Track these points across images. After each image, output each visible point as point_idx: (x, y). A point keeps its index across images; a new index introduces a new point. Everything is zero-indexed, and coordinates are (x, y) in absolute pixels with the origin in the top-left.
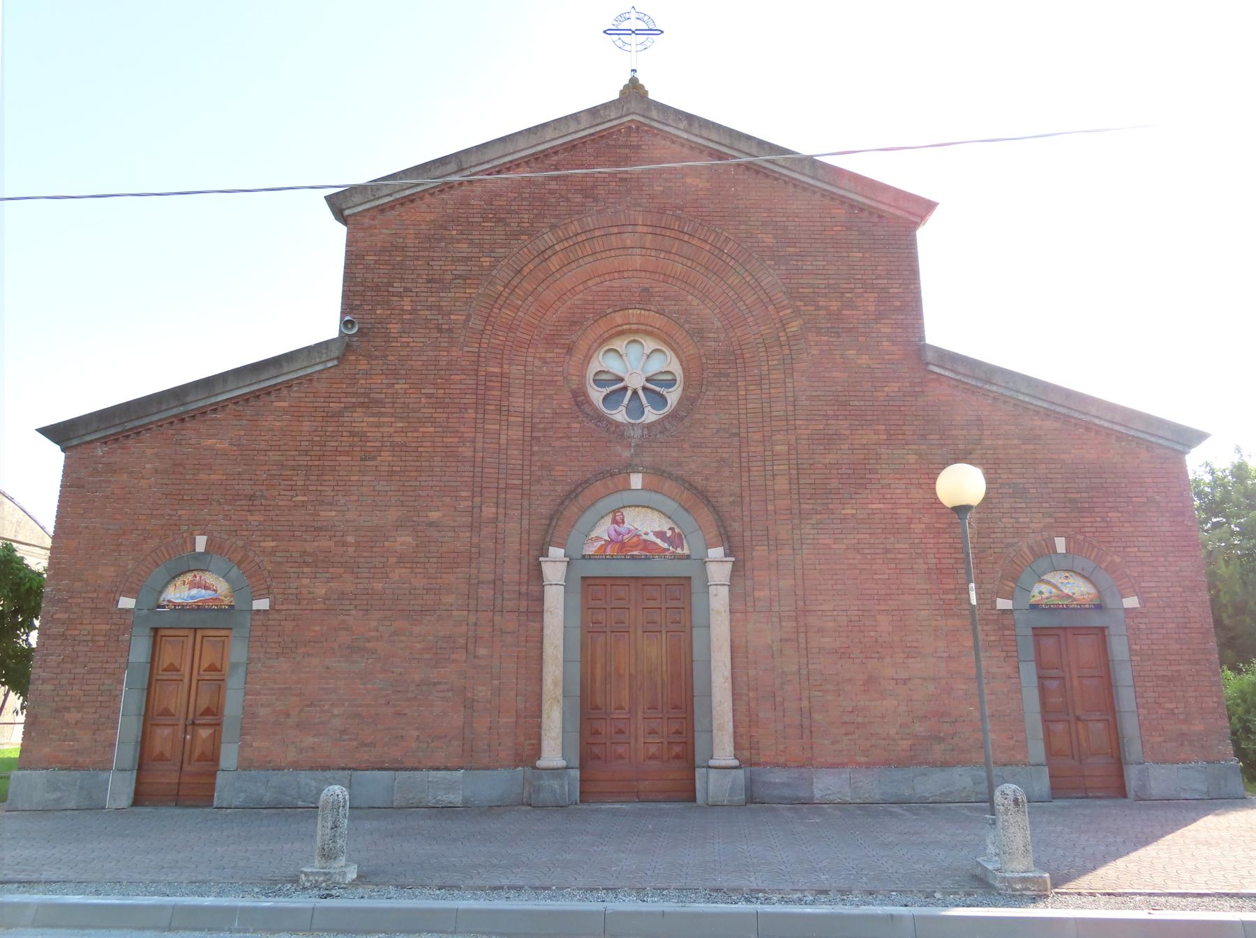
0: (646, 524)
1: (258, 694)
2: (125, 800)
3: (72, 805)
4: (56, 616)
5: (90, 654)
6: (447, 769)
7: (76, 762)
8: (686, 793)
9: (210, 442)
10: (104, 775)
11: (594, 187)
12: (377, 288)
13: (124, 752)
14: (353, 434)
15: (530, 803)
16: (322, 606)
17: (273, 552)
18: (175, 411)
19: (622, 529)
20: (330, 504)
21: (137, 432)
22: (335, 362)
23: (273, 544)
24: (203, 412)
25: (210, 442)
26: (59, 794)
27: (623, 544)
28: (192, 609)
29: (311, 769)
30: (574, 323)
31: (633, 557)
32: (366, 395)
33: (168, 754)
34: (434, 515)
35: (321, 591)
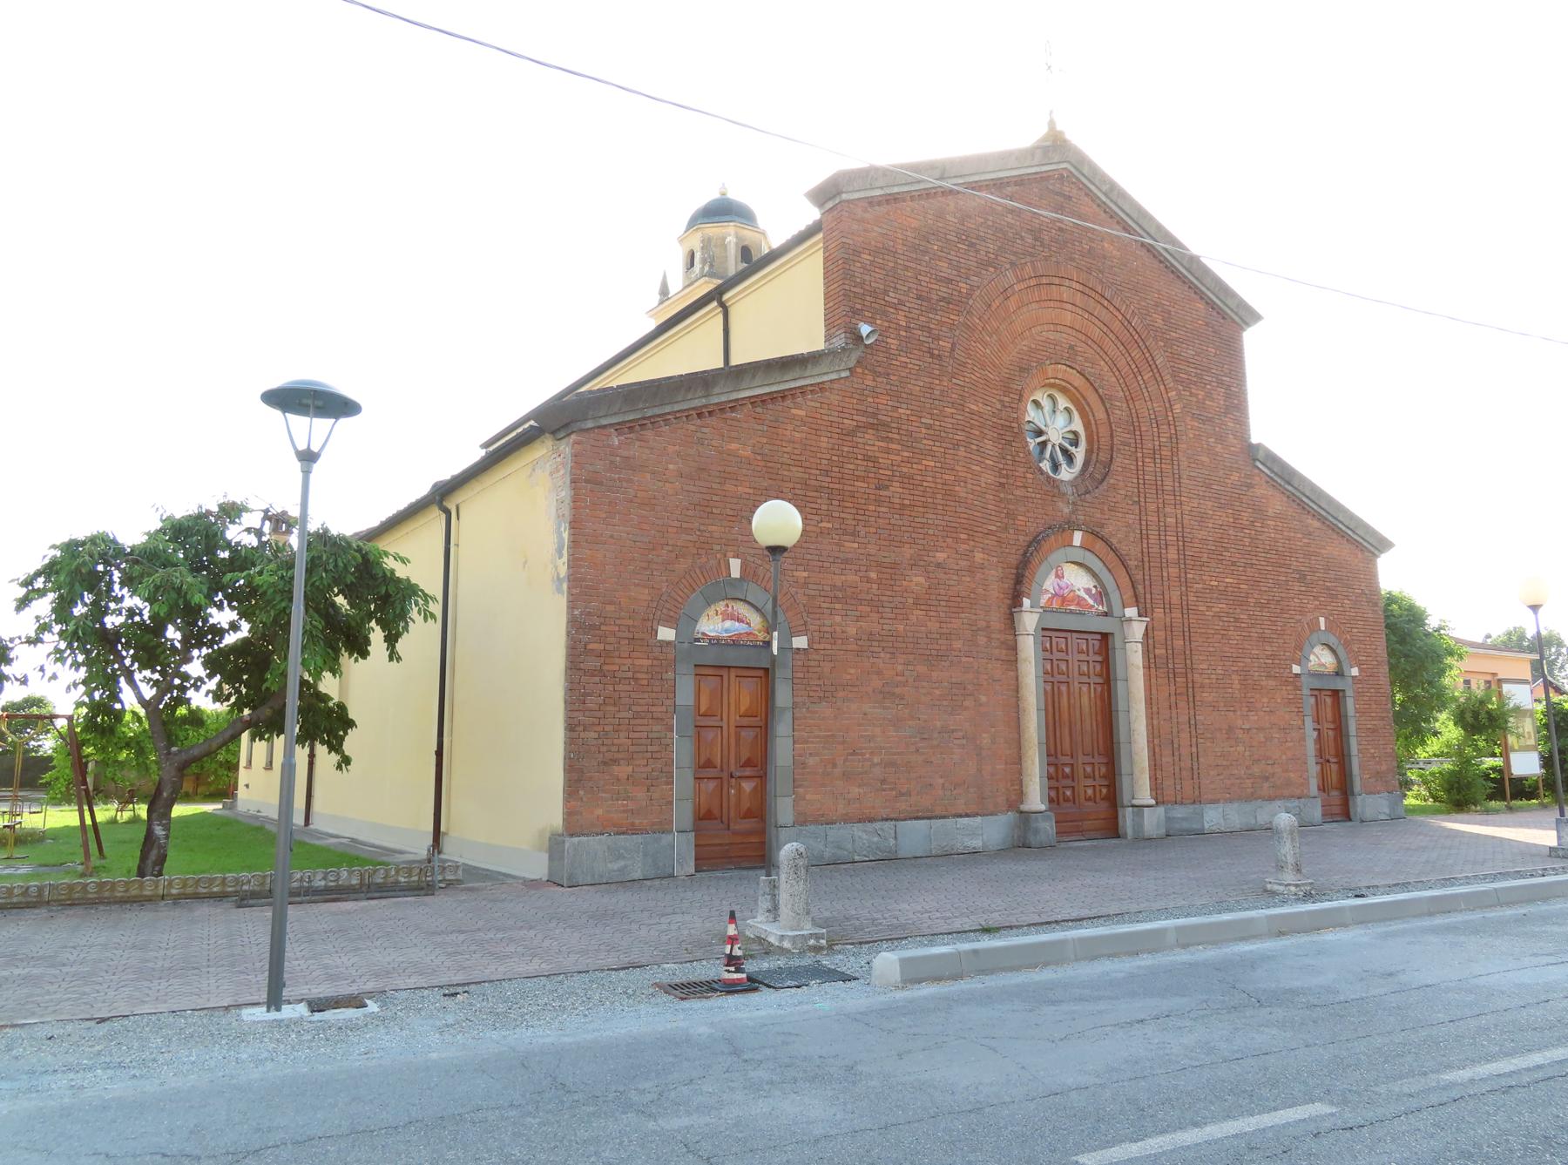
0: (1078, 581)
1: (806, 742)
2: (690, 868)
3: (637, 875)
4: (590, 646)
5: (633, 695)
6: (967, 815)
7: (633, 824)
8: (1112, 829)
9: (734, 446)
10: (666, 839)
11: (1040, 230)
12: (873, 293)
13: (682, 814)
14: (867, 458)
15: (1022, 844)
16: (854, 647)
17: (806, 584)
18: (697, 403)
19: (1062, 584)
20: (853, 534)
21: (653, 421)
22: (847, 374)
23: (805, 574)
24: (722, 408)
25: (734, 446)
26: (622, 863)
27: (1064, 599)
28: (727, 645)
29: (859, 821)
30: (1022, 370)
31: (1071, 612)
32: (874, 415)
33: (716, 812)
34: (941, 556)
35: (852, 631)
